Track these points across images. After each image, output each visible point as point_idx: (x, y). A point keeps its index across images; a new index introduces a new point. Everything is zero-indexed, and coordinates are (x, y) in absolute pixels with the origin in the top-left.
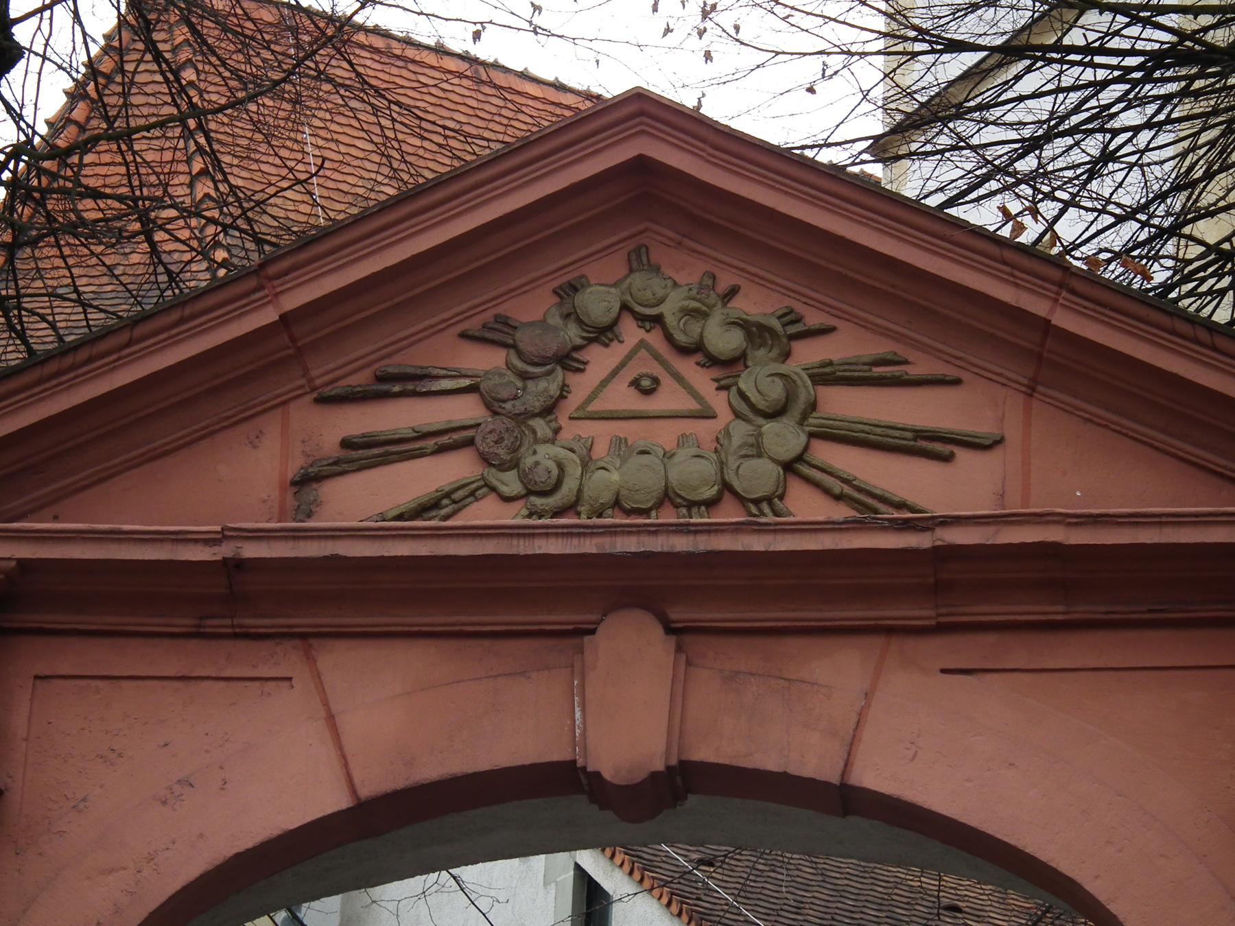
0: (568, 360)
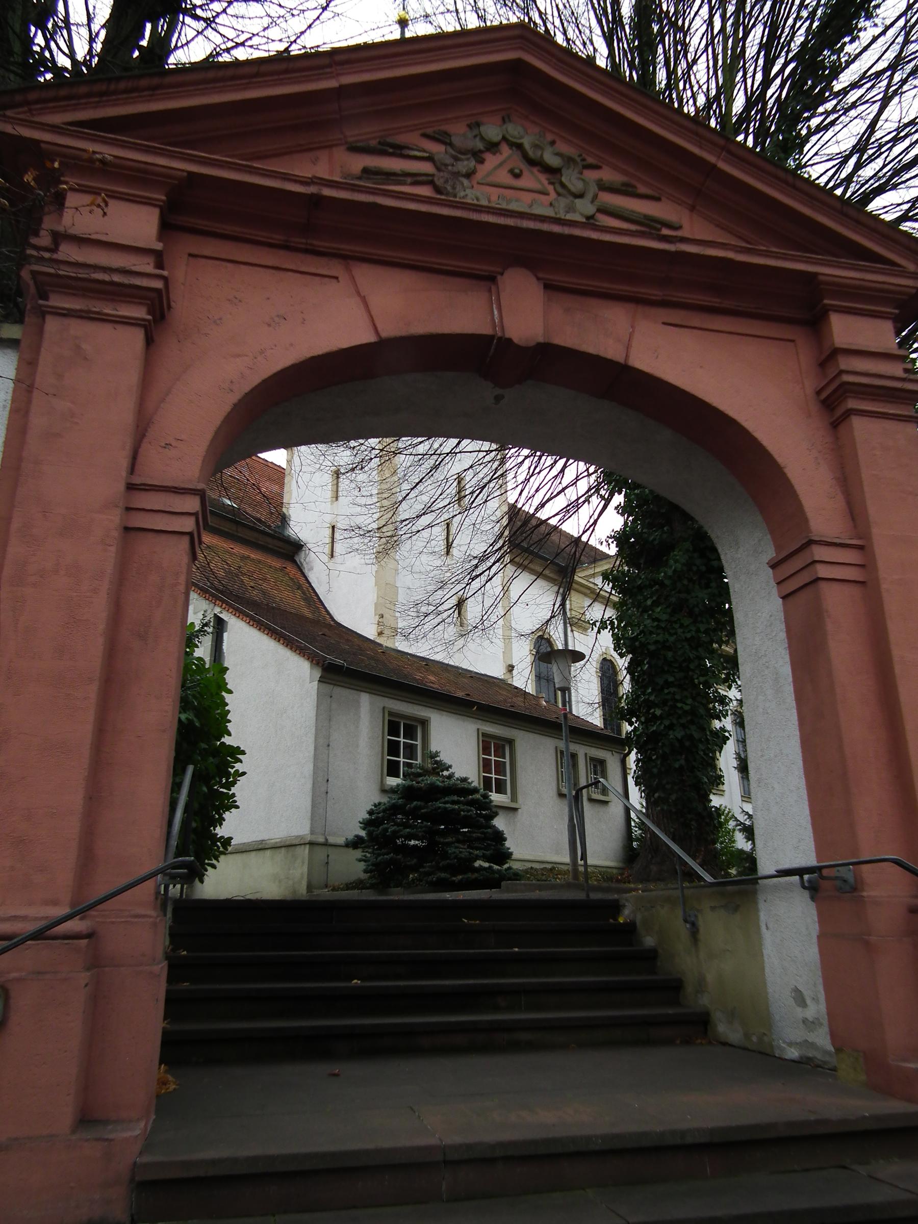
0: (478, 156)
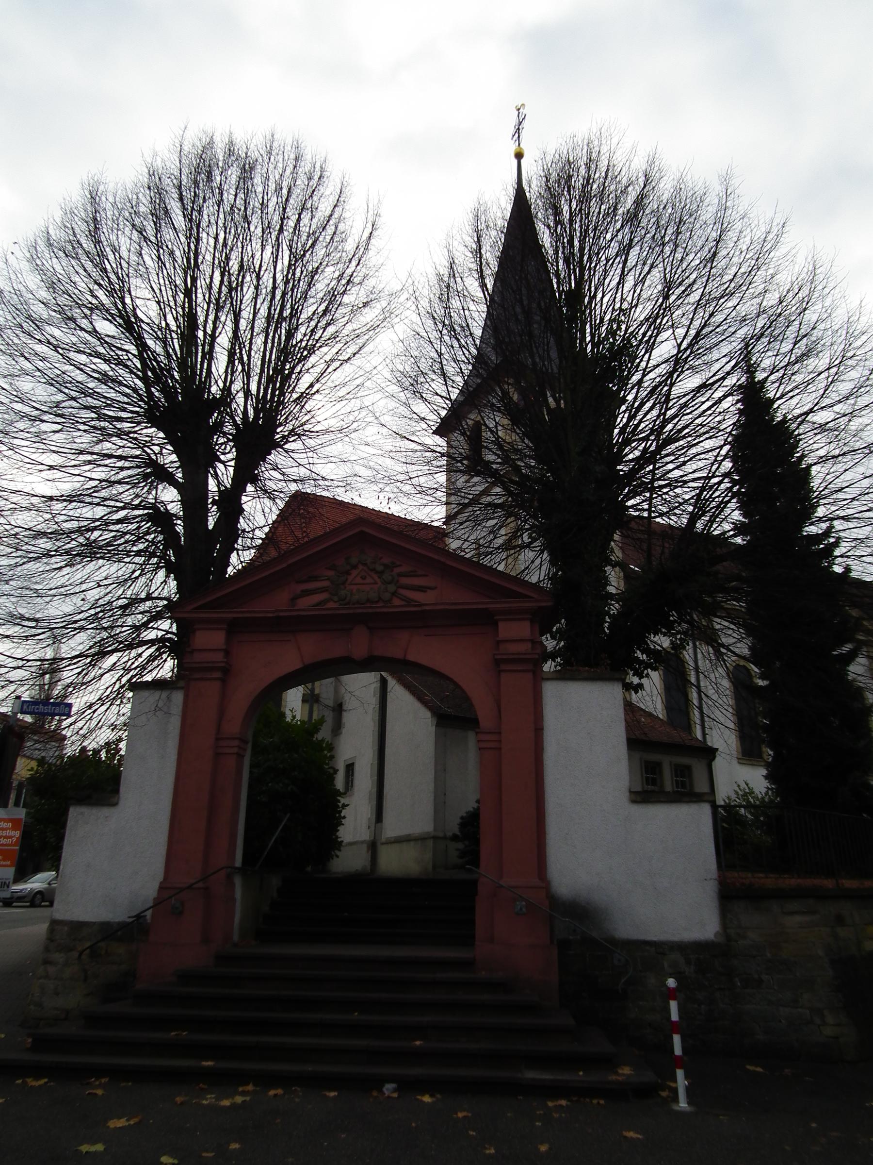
0: (348, 573)
